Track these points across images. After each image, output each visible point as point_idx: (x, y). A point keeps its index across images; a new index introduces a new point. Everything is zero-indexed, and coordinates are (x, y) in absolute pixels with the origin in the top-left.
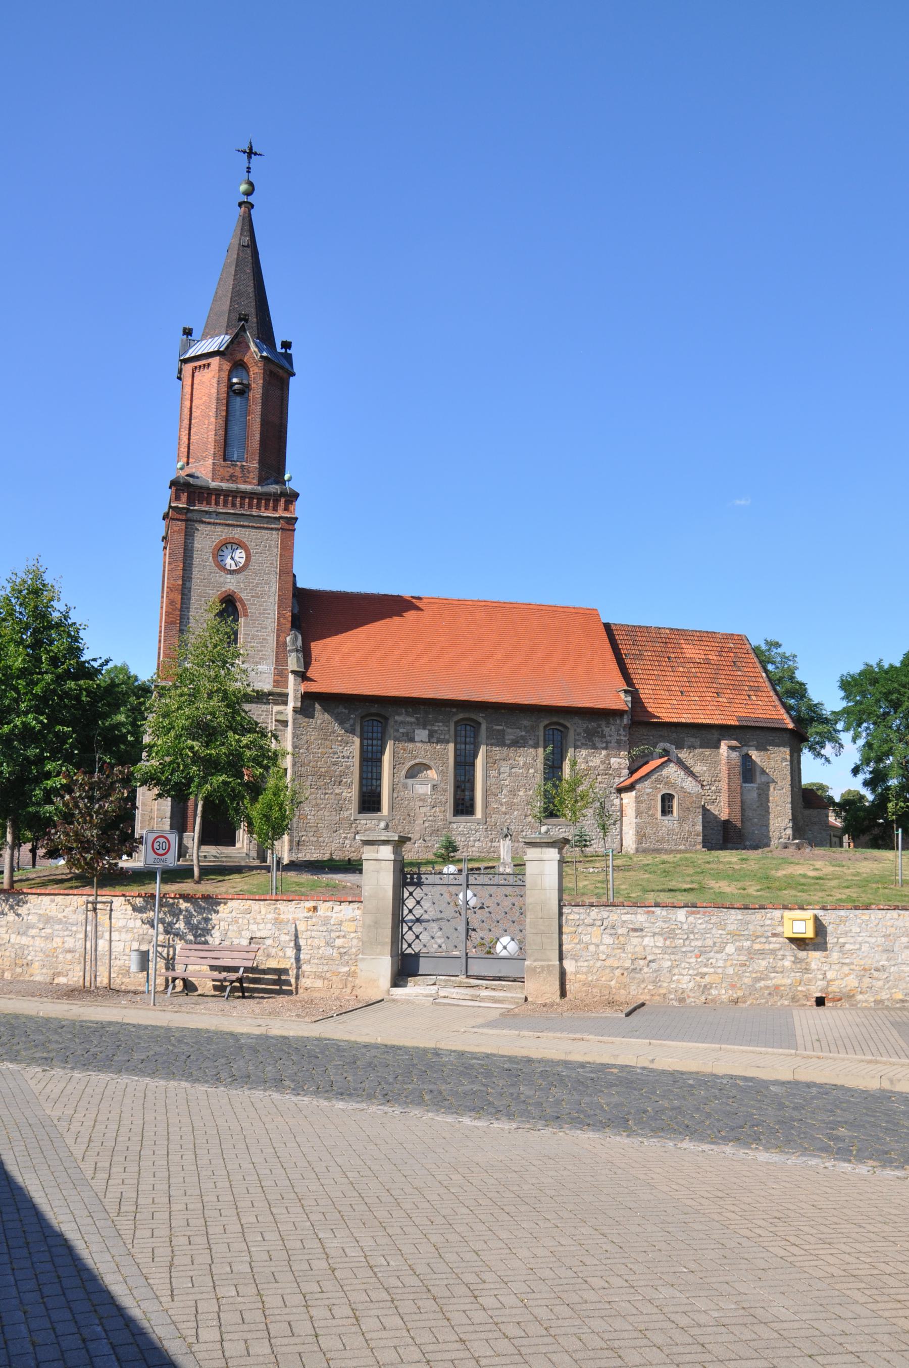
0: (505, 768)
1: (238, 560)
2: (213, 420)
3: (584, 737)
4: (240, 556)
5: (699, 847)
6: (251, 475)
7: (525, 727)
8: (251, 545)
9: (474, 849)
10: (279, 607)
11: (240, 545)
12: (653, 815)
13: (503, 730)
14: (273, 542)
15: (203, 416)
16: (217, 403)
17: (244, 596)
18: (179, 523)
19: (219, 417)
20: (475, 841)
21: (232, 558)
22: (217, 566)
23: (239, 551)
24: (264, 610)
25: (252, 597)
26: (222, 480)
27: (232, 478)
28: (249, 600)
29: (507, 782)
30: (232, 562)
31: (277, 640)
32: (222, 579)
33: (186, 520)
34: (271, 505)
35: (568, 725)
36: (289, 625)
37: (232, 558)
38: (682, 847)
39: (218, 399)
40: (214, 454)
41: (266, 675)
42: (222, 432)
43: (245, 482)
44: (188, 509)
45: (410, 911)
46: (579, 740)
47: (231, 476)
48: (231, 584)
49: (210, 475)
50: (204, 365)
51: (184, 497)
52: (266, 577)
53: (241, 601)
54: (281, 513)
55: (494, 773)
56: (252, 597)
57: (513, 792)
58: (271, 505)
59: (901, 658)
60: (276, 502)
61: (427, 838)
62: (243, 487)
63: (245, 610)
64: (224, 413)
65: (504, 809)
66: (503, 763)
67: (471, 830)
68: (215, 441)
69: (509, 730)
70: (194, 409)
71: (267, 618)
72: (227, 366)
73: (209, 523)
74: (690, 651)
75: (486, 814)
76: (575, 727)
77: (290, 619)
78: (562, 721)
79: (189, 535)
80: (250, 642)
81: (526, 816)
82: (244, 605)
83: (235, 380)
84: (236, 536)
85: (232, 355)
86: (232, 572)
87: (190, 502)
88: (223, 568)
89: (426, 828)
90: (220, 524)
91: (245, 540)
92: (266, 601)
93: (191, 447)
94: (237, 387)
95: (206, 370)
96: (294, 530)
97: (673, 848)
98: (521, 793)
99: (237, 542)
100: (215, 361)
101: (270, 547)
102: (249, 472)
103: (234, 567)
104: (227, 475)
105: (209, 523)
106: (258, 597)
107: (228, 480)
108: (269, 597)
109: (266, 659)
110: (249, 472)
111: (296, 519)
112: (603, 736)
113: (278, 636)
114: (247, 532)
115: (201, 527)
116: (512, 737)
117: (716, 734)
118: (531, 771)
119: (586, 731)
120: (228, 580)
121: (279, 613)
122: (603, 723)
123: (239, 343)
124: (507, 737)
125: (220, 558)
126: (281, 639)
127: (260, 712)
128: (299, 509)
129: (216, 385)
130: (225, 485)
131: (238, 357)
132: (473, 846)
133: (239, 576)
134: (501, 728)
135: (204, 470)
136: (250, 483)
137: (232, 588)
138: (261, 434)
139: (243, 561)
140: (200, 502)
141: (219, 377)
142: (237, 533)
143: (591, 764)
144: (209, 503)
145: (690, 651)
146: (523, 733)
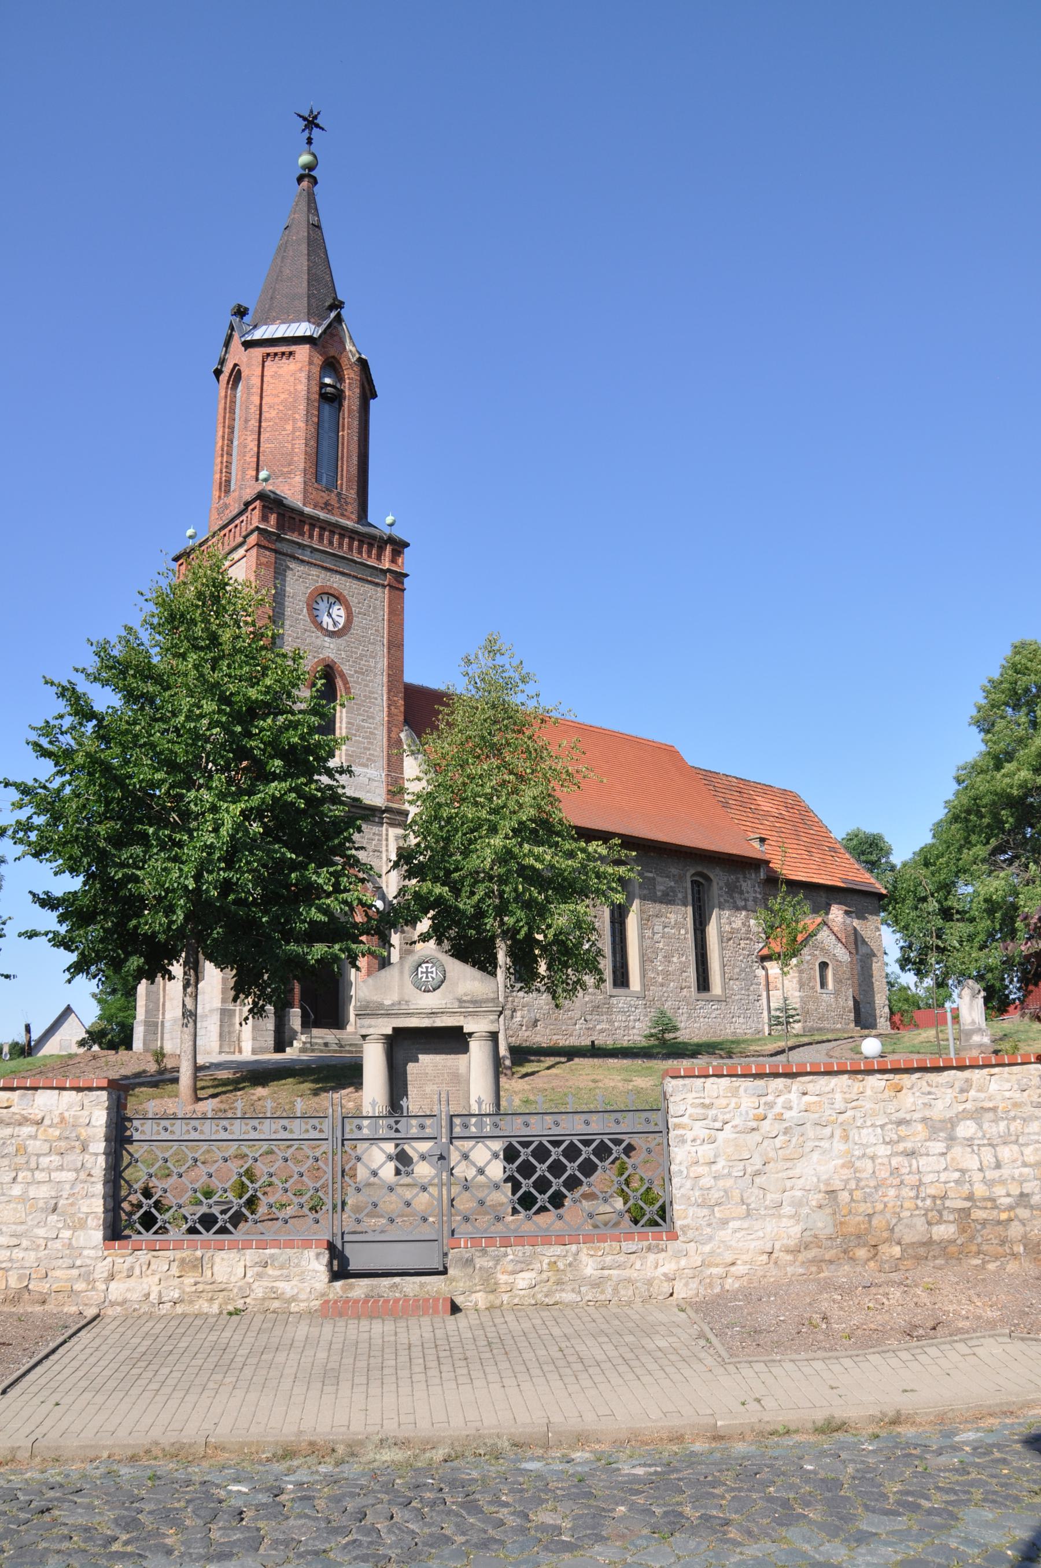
0: (658, 928)
1: (337, 619)
2: (301, 424)
3: (726, 893)
4: (339, 612)
5: (852, 1025)
6: (350, 508)
7: (674, 876)
8: (353, 601)
9: (635, 1031)
10: (389, 691)
11: (338, 598)
12: (813, 988)
13: (654, 879)
14: (378, 603)
15: (281, 419)
16: (308, 404)
17: (345, 669)
18: (268, 553)
19: (310, 422)
20: (635, 1020)
21: (330, 615)
22: (313, 622)
23: (337, 607)
24: (370, 692)
25: (356, 672)
26: (315, 507)
27: (327, 506)
28: (352, 676)
29: (661, 945)
30: (330, 621)
31: (389, 737)
32: (319, 642)
33: (276, 551)
34: (374, 552)
35: (712, 876)
36: (401, 718)
37: (330, 615)
38: (839, 1026)
39: (308, 399)
40: (305, 470)
41: (376, 784)
42: (313, 443)
43: (343, 515)
44: (278, 536)
45: (466, 1157)
46: (722, 896)
47: (327, 504)
48: (330, 650)
49: (301, 496)
50: (283, 354)
51: (273, 518)
52: (371, 648)
53: (343, 676)
54: (386, 565)
55: (648, 933)
56: (356, 672)
57: (667, 958)
58: (374, 552)
59: (931, 835)
60: (381, 550)
61: (588, 1017)
62: (343, 521)
63: (348, 690)
64: (316, 420)
65: (660, 980)
66: (656, 920)
67: (631, 1006)
68: (306, 453)
69: (659, 879)
70: (265, 408)
71: (374, 704)
72: (318, 360)
73: (303, 561)
74: (765, 805)
75: (644, 985)
76: (719, 879)
77: (402, 709)
78: (705, 871)
79: (280, 573)
80: (355, 735)
81: (682, 989)
82: (346, 683)
83: (327, 381)
84: (335, 585)
85: (324, 347)
86: (332, 634)
87: (280, 525)
88: (319, 625)
89: (587, 1003)
90: (315, 565)
91: (345, 593)
92: (372, 681)
93: (262, 458)
94: (329, 389)
95: (284, 360)
96: (403, 590)
97: (832, 1027)
98: (675, 959)
99: (336, 593)
100: (303, 351)
101: (375, 608)
102: (347, 503)
103: (331, 628)
104: (322, 501)
105: (303, 561)
106: (363, 673)
107: (322, 509)
108: (375, 675)
109: (375, 762)
110: (347, 503)
111: (406, 575)
112: (741, 893)
113: (389, 731)
114: (355, 585)
115: (292, 565)
116: (662, 888)
117: (822, 898)
118: (683, 932)
119: (727, 885)
120: (327, 645)
121: (389, 699)
122: (741, 876)
123: (332, 335)
124: (658, 887)
125: (316, 613)
126: (393, 735)
127: (371, 836)
128: (408, 562)
129: (305, 381)
130: (322, 515)
131: (332, 352)
132: (634, 1028)
133: (339, 641)
134: (650, 875)
135: (292, 490)
136: (349, 518)
137: (332, 656)
138: (359, 457)
139: (342, 621)
140: (293, 531)
141: (309, 372)
142: (336, 582)
143: (734, 926)
144: (302, 534)
145: (765, 805)
146: (672, 884)
